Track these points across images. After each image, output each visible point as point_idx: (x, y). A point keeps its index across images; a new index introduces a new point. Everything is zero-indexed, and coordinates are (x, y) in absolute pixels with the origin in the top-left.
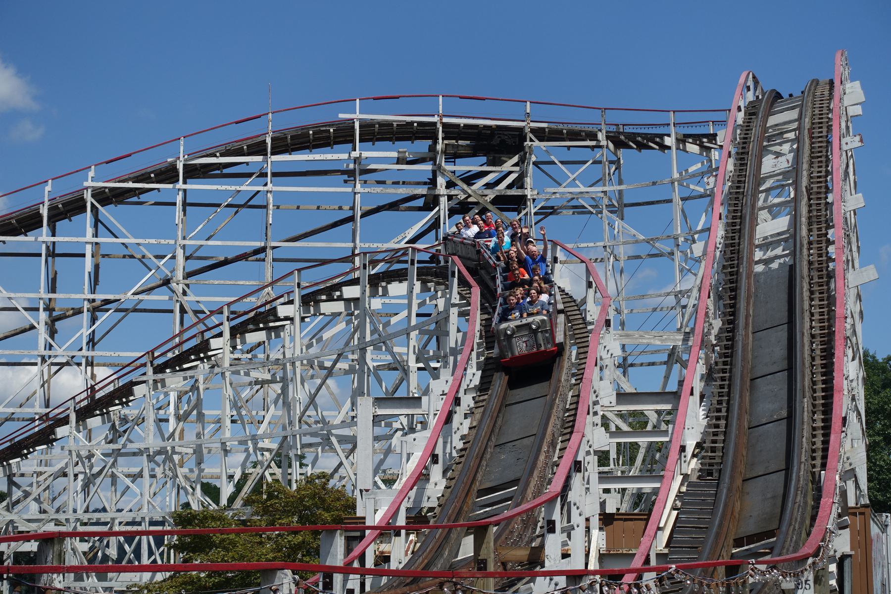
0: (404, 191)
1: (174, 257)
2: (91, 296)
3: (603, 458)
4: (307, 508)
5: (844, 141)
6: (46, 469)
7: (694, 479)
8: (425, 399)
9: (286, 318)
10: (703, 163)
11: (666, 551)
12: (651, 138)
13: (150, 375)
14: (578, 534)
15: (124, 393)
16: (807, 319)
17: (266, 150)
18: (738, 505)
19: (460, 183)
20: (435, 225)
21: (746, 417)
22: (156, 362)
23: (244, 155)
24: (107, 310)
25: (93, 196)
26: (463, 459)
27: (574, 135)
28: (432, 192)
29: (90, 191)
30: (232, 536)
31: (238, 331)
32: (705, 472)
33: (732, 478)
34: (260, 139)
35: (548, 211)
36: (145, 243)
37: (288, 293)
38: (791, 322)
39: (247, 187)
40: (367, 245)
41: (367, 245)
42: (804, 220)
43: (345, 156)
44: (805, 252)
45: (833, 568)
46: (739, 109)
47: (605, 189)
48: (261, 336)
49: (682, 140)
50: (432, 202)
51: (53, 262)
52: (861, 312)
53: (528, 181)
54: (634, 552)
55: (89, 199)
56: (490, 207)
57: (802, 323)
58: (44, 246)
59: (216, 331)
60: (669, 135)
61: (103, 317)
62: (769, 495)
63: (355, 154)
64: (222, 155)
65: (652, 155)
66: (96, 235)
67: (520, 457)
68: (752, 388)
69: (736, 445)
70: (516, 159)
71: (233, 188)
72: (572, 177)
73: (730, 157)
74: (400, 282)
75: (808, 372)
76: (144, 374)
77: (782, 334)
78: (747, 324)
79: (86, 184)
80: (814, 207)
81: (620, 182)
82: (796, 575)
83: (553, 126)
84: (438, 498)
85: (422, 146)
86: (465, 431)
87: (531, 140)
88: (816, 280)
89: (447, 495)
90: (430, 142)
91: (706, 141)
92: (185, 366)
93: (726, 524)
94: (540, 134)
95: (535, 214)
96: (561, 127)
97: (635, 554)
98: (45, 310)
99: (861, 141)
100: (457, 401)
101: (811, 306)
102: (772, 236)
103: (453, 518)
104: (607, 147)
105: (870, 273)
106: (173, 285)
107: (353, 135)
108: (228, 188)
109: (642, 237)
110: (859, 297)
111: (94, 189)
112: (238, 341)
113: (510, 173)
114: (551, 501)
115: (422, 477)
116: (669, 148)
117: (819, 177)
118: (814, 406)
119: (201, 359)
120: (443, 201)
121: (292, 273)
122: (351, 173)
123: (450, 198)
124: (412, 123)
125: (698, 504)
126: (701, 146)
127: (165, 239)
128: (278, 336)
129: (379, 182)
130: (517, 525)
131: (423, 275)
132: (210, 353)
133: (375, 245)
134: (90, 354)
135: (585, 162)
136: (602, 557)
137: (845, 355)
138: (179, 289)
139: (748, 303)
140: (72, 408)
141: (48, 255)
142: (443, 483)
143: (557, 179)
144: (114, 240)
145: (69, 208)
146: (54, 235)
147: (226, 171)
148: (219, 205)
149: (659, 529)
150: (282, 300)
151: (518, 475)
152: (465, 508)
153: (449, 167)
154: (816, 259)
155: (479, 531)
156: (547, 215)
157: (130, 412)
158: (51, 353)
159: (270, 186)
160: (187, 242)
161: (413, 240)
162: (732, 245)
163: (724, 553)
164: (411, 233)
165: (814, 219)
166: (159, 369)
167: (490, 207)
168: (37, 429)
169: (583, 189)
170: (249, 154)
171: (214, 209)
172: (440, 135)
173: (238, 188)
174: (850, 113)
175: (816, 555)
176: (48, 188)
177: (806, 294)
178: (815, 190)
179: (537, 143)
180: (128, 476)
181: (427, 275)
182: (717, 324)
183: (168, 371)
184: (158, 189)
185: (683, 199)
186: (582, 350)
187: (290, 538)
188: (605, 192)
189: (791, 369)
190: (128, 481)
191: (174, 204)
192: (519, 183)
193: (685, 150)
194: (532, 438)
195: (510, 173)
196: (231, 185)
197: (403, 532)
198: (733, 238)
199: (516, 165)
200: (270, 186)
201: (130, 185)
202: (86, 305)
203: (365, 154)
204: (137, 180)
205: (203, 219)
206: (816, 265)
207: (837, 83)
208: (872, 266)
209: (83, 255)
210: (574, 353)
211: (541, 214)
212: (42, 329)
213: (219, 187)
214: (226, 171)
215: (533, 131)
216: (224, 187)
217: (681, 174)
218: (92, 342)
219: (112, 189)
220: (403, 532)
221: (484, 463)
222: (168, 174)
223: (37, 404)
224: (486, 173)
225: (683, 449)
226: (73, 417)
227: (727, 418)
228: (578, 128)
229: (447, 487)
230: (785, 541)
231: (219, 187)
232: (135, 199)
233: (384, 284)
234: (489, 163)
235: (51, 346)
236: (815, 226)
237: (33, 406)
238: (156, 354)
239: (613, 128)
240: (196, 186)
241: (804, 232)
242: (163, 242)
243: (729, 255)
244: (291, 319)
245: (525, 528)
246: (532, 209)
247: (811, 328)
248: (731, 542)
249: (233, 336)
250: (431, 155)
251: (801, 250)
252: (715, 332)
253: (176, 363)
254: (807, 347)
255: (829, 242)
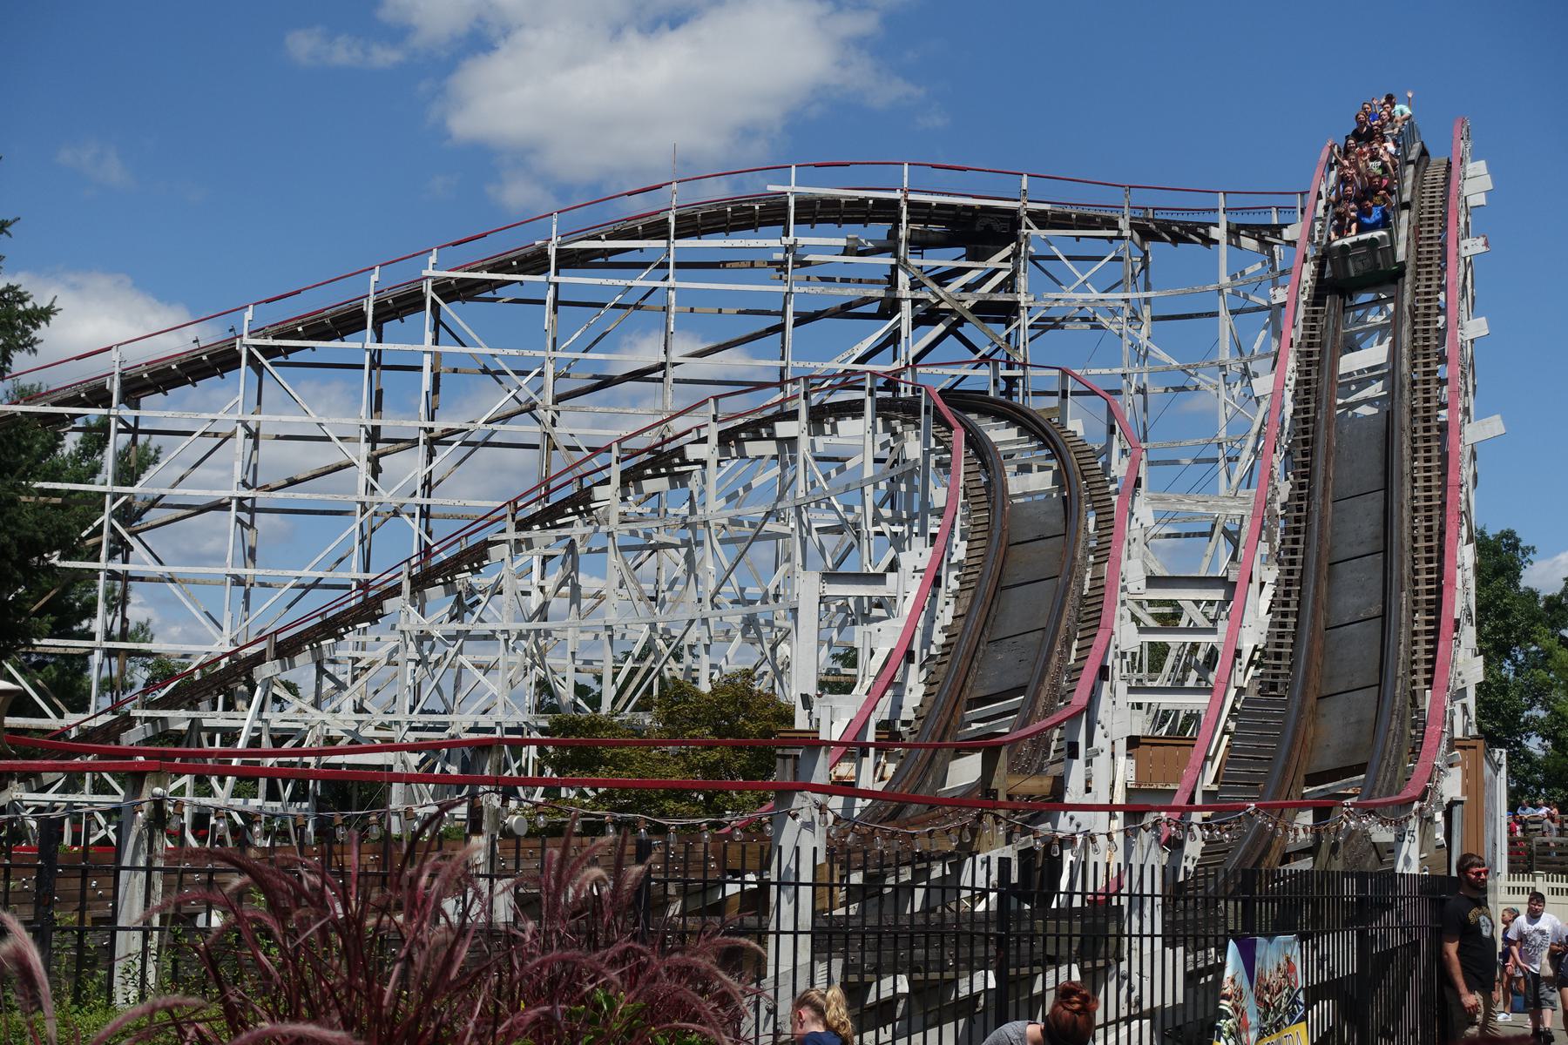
0: (852, 292)
1: (541, 374)
2: (429, 425)
3: (1135, 664)
4: (726, 717)
5: (1463, 243)
6: (364, 654)
7: (1252, 694)
8: (890, 576)
9: (696, 462)
10: (1264, 264)
11: (1215, 788)
12: (1192, 228)
13: (512, 535)
14: (1101, 762)
15: (476, 556)
16: (1407, 485)
17: (668, 232)
18: (1311, 730)
19: (929, 283)
20: (894, 338)
21: (1322, 615)
22: (521, 516)
23: (637, 238)
24: (450, 443)
25: (434, 289)
26: (947, 658)
27: (1086, 222)
28: (892, 295)
29: (430, 282)
30: (626, 751)
31: (631, 478)
32: (1268, 686)
33: (1304, 694)
34: (661, 217)
35: (1046, 325)
36: (503, 354)
37: (698, 428)
38: (1387, 488)
39: (641, 281)
40: (801, 364)
41: (801, 364)
42: (1405, 351)
43: (776, 243)
44: (1406, 394)
45: (1439, 817)
46: (1319, 196)
47: (1127, 296)
48: (662, 484)
49: (1234, 232)
50: (890, 308)
51: (379, 376)
52: (1475, 476)
53: (1022, 281)
54: (1172, 787)
55: (428, 289)
56: (969, 316)
57: (1401, 491)
58: (367, 355)
59: (598, 477)
60: (1217, 225)
61: (443, 453)
62: (1352, 720)
63: (789, 241)
64: (608, 238)
65: (1191, 251)
66: (436, 342)
67: (1024, 657)
68: (1331, 576)
69: (1310, 651)
70: (1007, 251)
71: (623, 283)
72: (1082, 279)
73: (1305, 261)
74: (854, 417)
75: (1407, 556)
76: (504, 531)
77: (1375, 503)
78: (1325, 490)
79: (425, 273)
80: (1420, 335)
81: (1147, 288)
82: (1398, 824)
83: (1059, 209)
84: (915, 710)
85: (880, 231)
86: (948, 621)
87: (1028, 227)
88: (1420, 433)
89: (928, 704)
90: (889, 226)
91: (1266, 234)
92: (559, 522)
93: (1296, 755)
94: (1041, 220)
95: (1031, 327)
96: (1068, 210)
97: (1175, 791)
98: (367, 441)
99: (1486, 244)
100: (937, 582)
101: (1413, 468)
102: (1360, 372)
103: (939, 734)
104: (1131, 238)
105: (1494, 426)
106: (539, 412)
107: (786, 215)
108: (616, 282)
109: (1175, 363)
110: (1474, 455)
111: (436, 280)
112: (632, 490)
113: (997, 271)
114: (1076, 717)
115: (892, 683)
116: (1216, 242)
117: (1428, 293)
118: (1416, 603)
119: (580, 514)
120: (906, 306)
121: (706, 401)
122: (781, 266)
123: (915, 302)
124: (867, 199)
125: (1256, 727)
126: (1261, 241)
127: (530, 349)
128: (684, 485)
129: (823, 279)
130: (1025, 748)
131: (882, 408)
132: (593, 506)
133: (812, 365)
134: (426, 501)
135: (1100, 259)
136: (1129, 791)
137: (1459, 536)
138: (548, 416)
139: (1327, 461)
140: (405, 574)
141: (372, 368)
142: (922, 689)
143: (1067, 284)
144: (461, 349)
145: (402, 305)
146: (379, 341)
147: (612, 259)
148: (603, 305)
149: (1207, 758)
150: (690, 437)
151: (1021, 681)
152: (953, 723)
153: (915, 261)
154: (1421, 404)
155: (990, 748)
156: (1045, 329)
157: (481, 581)
158: (375, 499)
159: (671, 282)
160: (558, 354)
161: (862, 360)
162: (1307, 382)
163: (1293, 793)
164: (861, 349)
165: (1420, 351)
166: (523, 525)
167: (969, 316)
168: (353, 603)
169: (1096, 295)
170: (644, 237)
171: (596, 310)
172: (904, 217)
173: (629, 283)
174: (1471, 203)
175: (1422, 799)
176: (374, 277)
177: (1407, 452)
178: (1422, 311)
179: (1035, 231)
180: (479, 667)
181: (890, 409)
182: (1285, 489)
183: (537, 527)
184: (521, 282)
185: (1233, 312)
186: (1102, 518)
187: (704, 754)
188: (1127, 301)
189: (1386, 547)
190: (479, 674)
191: (544, 302)
192: (1009, 284)
193: (1239, 246)
194: (1039, 634)
195: (997, 271)
196: (620, 278)
197: (872, 750)
198: (1308, 373)
199: (1006, 260)
200: (671, 282)
201: (485, 275)
202: (423, 436)
203: (802, 241)
204: (493, 269)
205: (582, 325)
206: (1422, 414)
207: (1455, 165)
208: (1498, 417)
209: (420, 368)
210: (1092, 521)
211: (1039, 327)
212: (364, 467)
213: (604, 281)
214: (612, 259)
215: (1030, 214)
216: (610, 282)
217: (1233, 277)
218: (428, 485)
219: (460, 281)
220: (872, 750)
221: (975, 664)
222: (535, 262)
223: (354, 564)
224: (965, 270)
225: (1238, 653)
226: (406, 586)
227: (1297, 615)
228: (1091, 212)
229: (926, 695)
230: (1376, 780)
231: (604, 281)
232: (489, 294)
233: (832, 420)
234: (969, 258)
235: (373, 488)
236: (1420, 360)
237: (349, 570)
238: (520, 504)
239: (1139, 214)
240: (569, 279)
241: (1405, 368)
242: (526, 353)
243: (1302, 396)
244: (704, 463)
245: (1035, 752)
246: (1024, 320)
247: (1414, 498)
248: (1302, 778)
249: (624, 484)
250: (891, 243)
251: (1401, 392)
252: (1283, 496)
253: (548, 518)
254: (1406, 524)
255: (1442, 382)
